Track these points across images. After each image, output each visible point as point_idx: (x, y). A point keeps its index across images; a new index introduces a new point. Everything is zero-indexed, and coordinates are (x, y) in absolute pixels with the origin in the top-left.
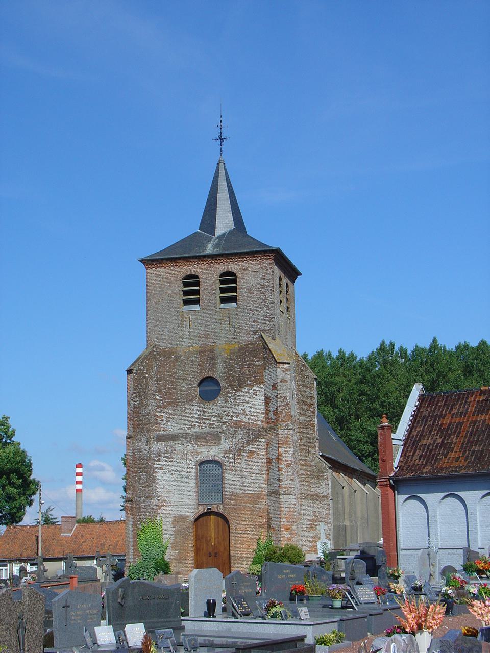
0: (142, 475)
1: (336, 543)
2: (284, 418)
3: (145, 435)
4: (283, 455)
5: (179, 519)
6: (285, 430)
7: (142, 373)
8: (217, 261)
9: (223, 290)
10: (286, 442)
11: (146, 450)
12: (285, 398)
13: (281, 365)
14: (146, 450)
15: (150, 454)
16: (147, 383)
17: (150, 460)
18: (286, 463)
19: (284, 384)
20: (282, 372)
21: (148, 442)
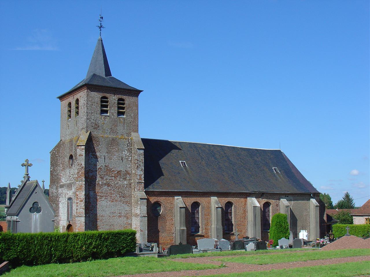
0: (53, 205)
1: (308, 239)
2: (80, 175)
3: (55, 185)
4: (78, 195)
5: (64, 226)
6: (80, 182)
7: (55, 155)
8: (110, 93)
9: (123, 108)
10: (81, 189)
11: (55, 193)
12: (81, 164)
13: (80, 147)
14: (55, 193)
15: (58, 195)
16: (57, 159)
17: (57, 198)
18: (80, 200)
19: (81, 157)
20: (80, 151)
21: (57, 188)
